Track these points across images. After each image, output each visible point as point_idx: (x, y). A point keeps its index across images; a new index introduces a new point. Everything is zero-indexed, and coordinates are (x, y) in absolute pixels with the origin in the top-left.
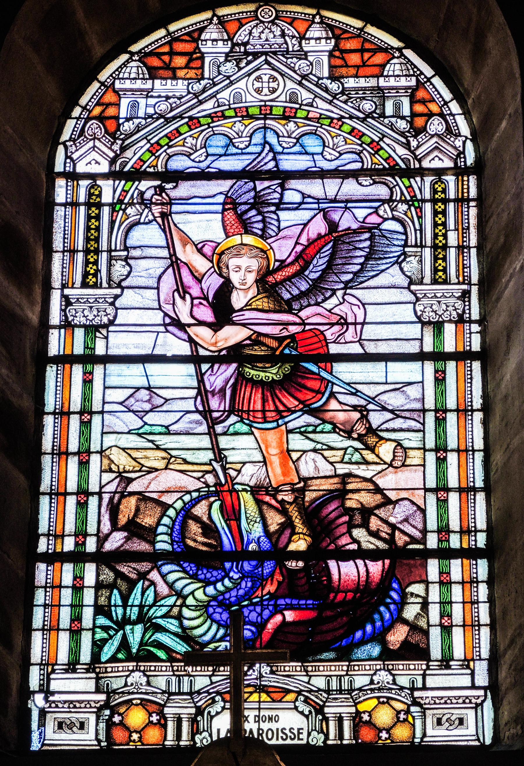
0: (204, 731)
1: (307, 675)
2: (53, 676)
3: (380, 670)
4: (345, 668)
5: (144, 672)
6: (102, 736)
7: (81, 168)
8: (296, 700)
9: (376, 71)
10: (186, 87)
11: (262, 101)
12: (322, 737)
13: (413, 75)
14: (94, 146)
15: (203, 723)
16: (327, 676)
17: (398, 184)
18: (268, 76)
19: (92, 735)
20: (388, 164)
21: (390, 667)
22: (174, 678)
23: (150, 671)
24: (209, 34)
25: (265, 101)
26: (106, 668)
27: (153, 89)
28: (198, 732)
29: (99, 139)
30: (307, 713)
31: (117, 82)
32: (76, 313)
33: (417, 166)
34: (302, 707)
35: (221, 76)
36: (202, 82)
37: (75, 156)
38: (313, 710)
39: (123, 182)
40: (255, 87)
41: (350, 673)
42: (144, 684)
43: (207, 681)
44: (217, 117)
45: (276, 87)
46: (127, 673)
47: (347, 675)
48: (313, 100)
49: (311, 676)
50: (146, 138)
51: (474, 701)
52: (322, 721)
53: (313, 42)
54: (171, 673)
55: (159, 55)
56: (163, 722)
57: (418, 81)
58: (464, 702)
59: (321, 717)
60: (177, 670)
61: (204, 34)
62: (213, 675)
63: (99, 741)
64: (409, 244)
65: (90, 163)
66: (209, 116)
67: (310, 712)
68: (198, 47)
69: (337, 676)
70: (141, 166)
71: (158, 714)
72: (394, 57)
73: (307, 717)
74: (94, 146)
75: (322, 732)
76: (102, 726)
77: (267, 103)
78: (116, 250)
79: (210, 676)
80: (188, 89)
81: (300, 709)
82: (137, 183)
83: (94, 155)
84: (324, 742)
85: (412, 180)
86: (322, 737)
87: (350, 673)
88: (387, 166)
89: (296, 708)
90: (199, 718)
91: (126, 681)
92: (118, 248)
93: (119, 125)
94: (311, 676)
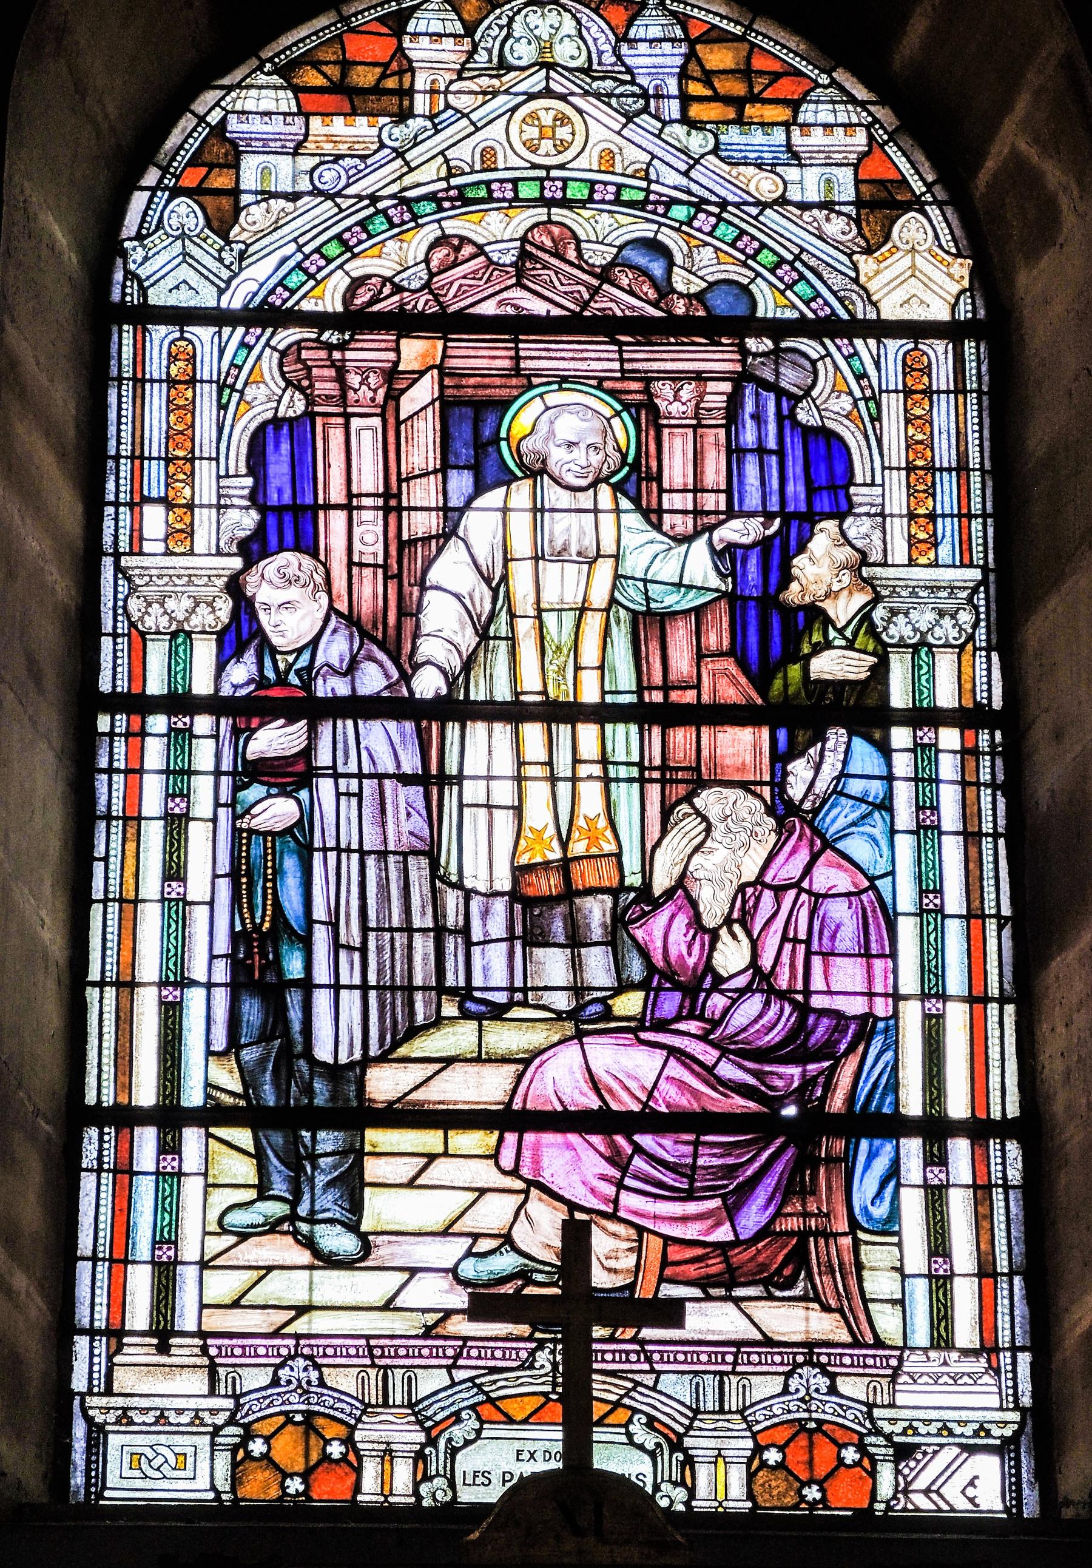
0: (438, 1475)
1: (652, 1371)
2: (117, 1359)
3: (801, 1366)
4: (729, 1358)
5: (310, 1358)
6: (223, 1485)
7: (157, 297)
8: (630, 1421)
9: (781, 113)
10: (375, 131)
11: (535, 166)
12: (680, 1494)
13: (860, 125)
14: (913, 266)
15: (437, 1461)
16: (696, 1373)
17: (829, 354)
18: (552, 113)
19: (203, 1482)
20: (814, 312)
21: (824, 1359)
22: (372, 1372)
23: (325, 1355)
24: (642, 30)
25: (549, 168)
26: (256, 1347)
27: (306, 135)
28: (427, 1478)
29: (190, 238)
30: (650, 1446)
31: (233, 119)
32: (150, 605)
33: (874, 316)
34: (641, 1434)
35: (450, 112)
36: (410, 122)
37: (143, 272)
38: (662, 1441)
39: (240, 331)
40: (525, 137)
41: (739, 1369)
42: (824, 1390)
43: (776, 1384)
44: (447, 199)
45: (569, 138)
46: (278, 1361)
47: (734, 1372)
48: (649, 164)
49: (659, 1373)
50: (295, 240)
51: (996, 1432)
52: (683, 1465)
53: (425, 41)
54: (368, 1361)
55: (317, 65)
56: (352, 1457)
57: (871, 138)
58: (976, 1434)
59: (681, 1457)
60: (382, 1356)
61: (413, 21)
62: (454, 1366)
63: (218, 1493)
64: (223, 482)
65: (177, 287)
66: (432, 197)
67: (658, 1445)
68: (400, 49)
69: (715, 1373)
70: (285, 301)
71: (343, 1442)
72: (818, 85)
73: (652, 1455)
74: (185, 254)
75: (683, 1484)
76: (223, 1461)
77: (554, 173)
78: (227, 476)
79: (449, 1368)
80: (380, 141)
81: (637, 1439)
82: (269, 331)
83: (914, 286)
84: (687, 1504)
85: (858, 343)
86: (680, 1494)
87: (739, 1369)
88: (827, 342)
89: (630, 1436)
90: (427, 1451)
91: (786, 1385)
92: (231, 472)
93: (237, 210)
94: (659, 1373)
